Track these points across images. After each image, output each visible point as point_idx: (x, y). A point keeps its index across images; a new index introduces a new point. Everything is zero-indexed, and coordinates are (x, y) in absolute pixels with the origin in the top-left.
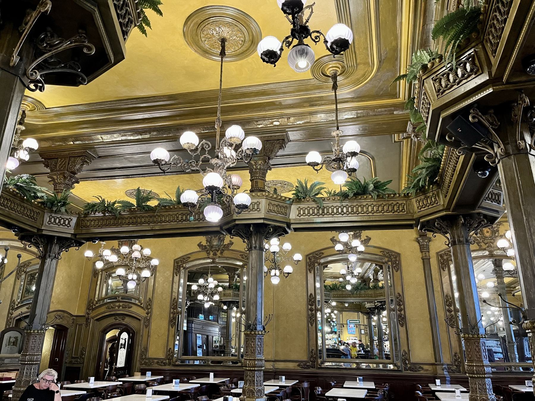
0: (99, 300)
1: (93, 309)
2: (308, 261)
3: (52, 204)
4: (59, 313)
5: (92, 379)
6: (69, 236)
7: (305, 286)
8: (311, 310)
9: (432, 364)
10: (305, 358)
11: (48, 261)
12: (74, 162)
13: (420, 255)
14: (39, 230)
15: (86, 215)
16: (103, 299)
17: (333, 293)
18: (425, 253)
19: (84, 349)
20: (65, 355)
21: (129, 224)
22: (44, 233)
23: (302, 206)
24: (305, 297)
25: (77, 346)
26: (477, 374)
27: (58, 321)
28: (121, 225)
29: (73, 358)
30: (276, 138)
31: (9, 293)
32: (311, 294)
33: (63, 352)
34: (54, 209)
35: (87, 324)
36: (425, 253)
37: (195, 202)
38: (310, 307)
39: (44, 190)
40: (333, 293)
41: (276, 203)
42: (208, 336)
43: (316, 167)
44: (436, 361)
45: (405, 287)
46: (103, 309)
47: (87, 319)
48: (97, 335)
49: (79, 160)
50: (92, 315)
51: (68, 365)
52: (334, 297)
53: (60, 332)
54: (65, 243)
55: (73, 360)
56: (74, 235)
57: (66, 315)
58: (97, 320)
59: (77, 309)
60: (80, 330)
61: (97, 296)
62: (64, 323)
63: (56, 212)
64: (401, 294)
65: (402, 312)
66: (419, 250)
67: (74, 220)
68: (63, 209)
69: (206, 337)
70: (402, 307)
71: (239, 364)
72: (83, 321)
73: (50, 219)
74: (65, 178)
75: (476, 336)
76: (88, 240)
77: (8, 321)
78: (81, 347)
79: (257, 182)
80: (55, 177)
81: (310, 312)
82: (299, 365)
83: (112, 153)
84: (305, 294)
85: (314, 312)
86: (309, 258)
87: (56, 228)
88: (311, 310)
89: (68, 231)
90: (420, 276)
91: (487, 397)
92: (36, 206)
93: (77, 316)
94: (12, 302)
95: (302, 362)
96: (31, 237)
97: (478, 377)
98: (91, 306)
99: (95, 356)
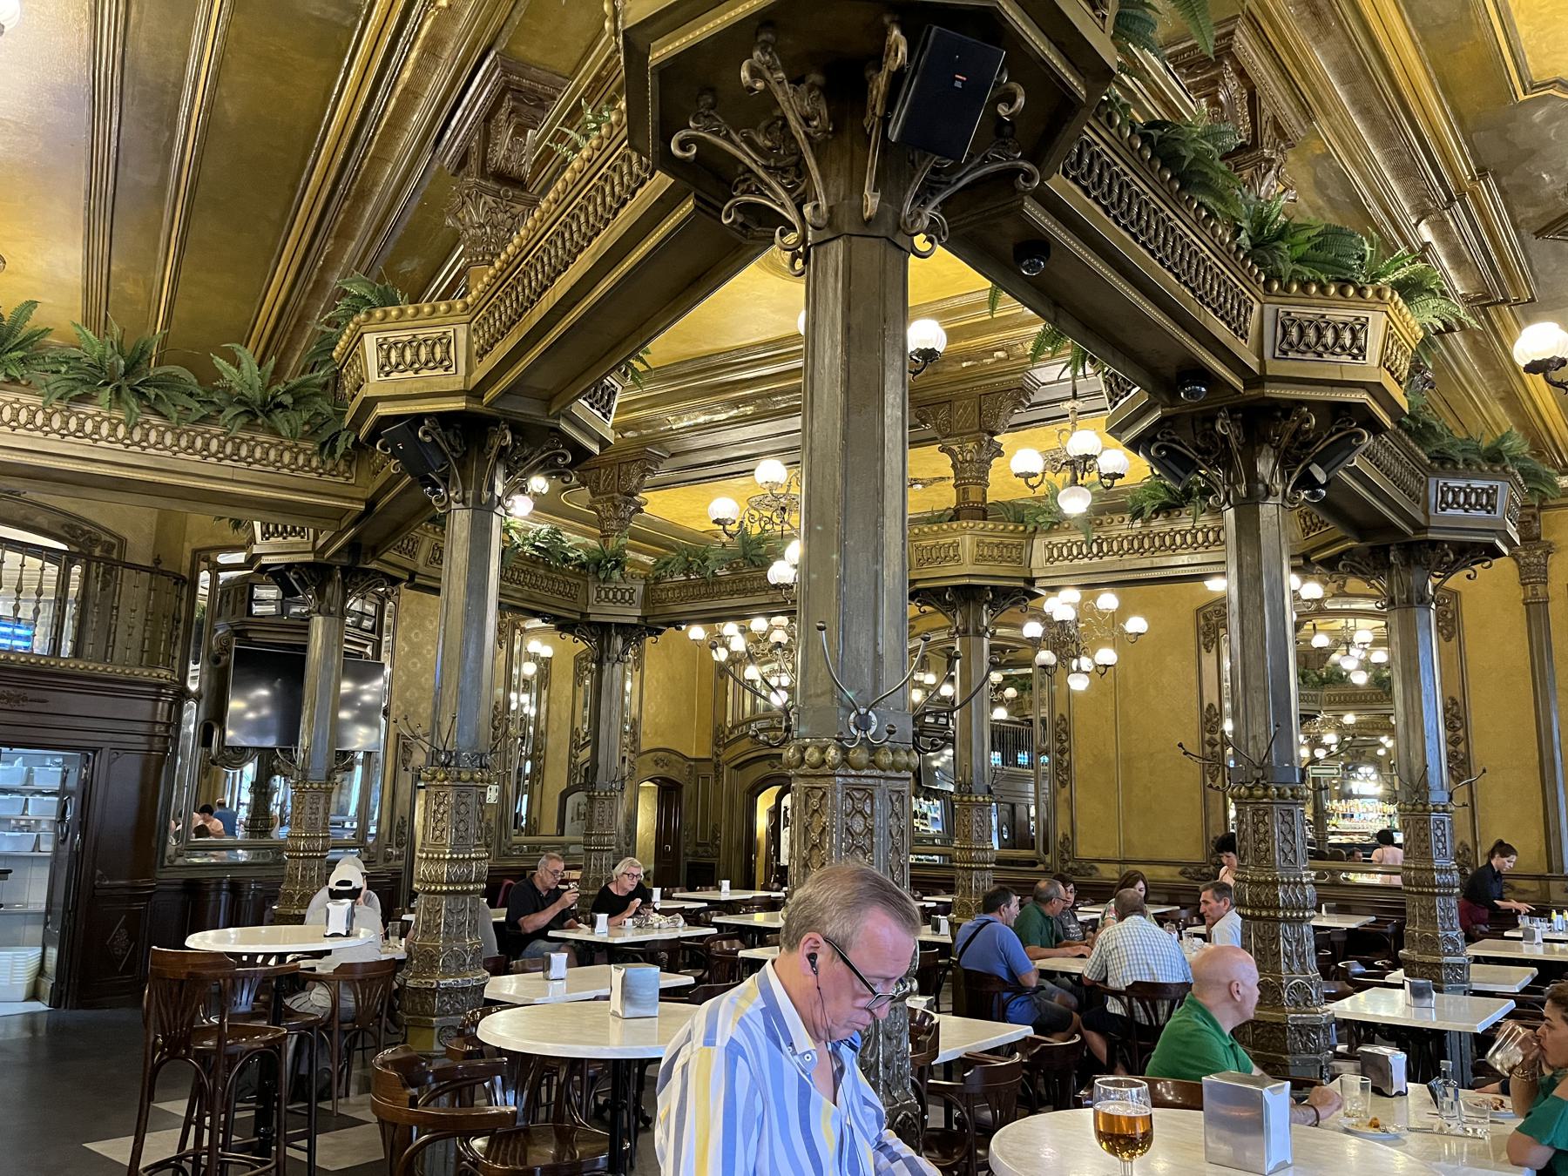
0: (734, 727)
1: (726, 746)
2: (1202, 622)
3: (598, 565)
4: (660, 754)
5: (726, 884)
6: (635, 621)
7: (1195, 684)
8: (1212, 744)
9: (1539, 878)
10: (1198, 857)
11: (607, 666)
12: (628, 473)
13: (1519, 593)
14: (583, 614)
15: (658, 580)
16: (748, 722)
17: (1326, 693)
18: (1534, 589)
19: (716, 829)
20: (683, 840)
21: (731, 593)
22: (593, 618)
23: (1055, 540)
24: (1195, 713)
25: (704, 820)
26: (1417, 885)
27: (661, 771)
28: (719, 595)
29: (698, 845)
30: (1002, 388)
31: (566, 715)
32: (1211, 706)
33: (678, 832)
34: (602, 576)
35: (718, 775)
36: (1534, 589)
37: (789, 581)
38: (1207, 736)
39: (578, 542)
40: (1326, 692)
41: (996, 540)
42: (1013, 806)
43: (1032, 481)
44: (1550, 871)
45: (1471, 680)
46: (744, 745)
47: (717, 766)
48: (739, 800)
49: (634, 469)
50: (724, 757)
51: (690, 860)
52: (1330, 703)
53: (669, 793)
54: (633, 633)
55: (700, 849)
56: (643, 618)
57: (674, 757)
58: (736, 767)
59: (695, 746)
60: (705, 789)
61: (729, 718)
62: (673, 774)
63: (604, 581)
64: (1459, 698)
65: (1462, 747)
66: (1517, 579)
67: (640, 588)
68: (616, 574)
69: (1008, 807)
70: (1461, 733)
71: (1040, 867)
72: (708, 770)
73: (599, 593)
74: (616, 507)
75: (1420, 807)
76: (669, 625)
77: (570, 771)
78: (710, 824)
79: (965, 492)
80: (599, 506)
81: (1208, 749)
82: (1182, 873)
83: (688, 448)
84: (1196, 705)
85: (1218, 748)
86: (1205, 617)
87: (610, 609)
88: (1212, 744)
89: (632, 614)
90: (1516, 649)
91: (1435, 934)
92: (573, 574)
93: (696, 760)
94: (574, 732)
95: (1190, 864)
96: (575, 626)
97: (1418, 893)
98: (720, 738)
99: (739, 843)
